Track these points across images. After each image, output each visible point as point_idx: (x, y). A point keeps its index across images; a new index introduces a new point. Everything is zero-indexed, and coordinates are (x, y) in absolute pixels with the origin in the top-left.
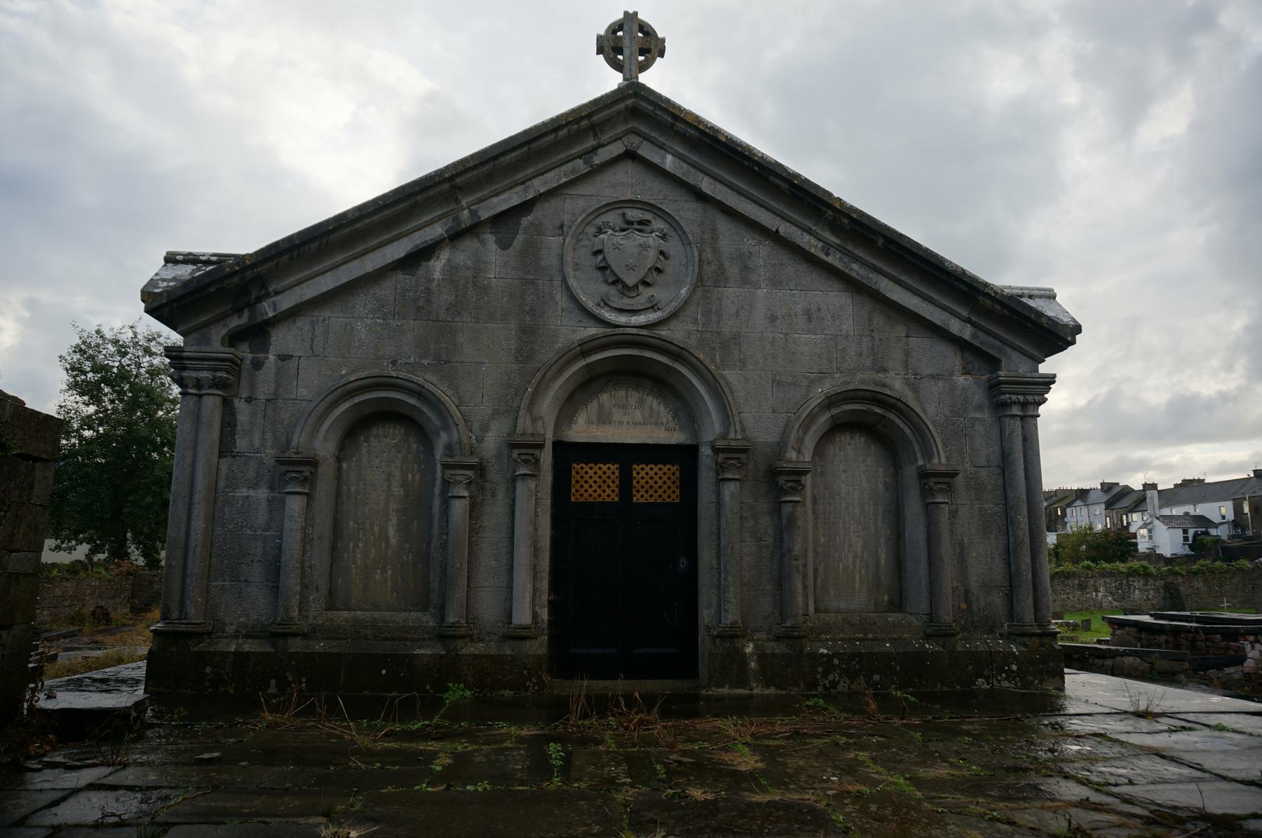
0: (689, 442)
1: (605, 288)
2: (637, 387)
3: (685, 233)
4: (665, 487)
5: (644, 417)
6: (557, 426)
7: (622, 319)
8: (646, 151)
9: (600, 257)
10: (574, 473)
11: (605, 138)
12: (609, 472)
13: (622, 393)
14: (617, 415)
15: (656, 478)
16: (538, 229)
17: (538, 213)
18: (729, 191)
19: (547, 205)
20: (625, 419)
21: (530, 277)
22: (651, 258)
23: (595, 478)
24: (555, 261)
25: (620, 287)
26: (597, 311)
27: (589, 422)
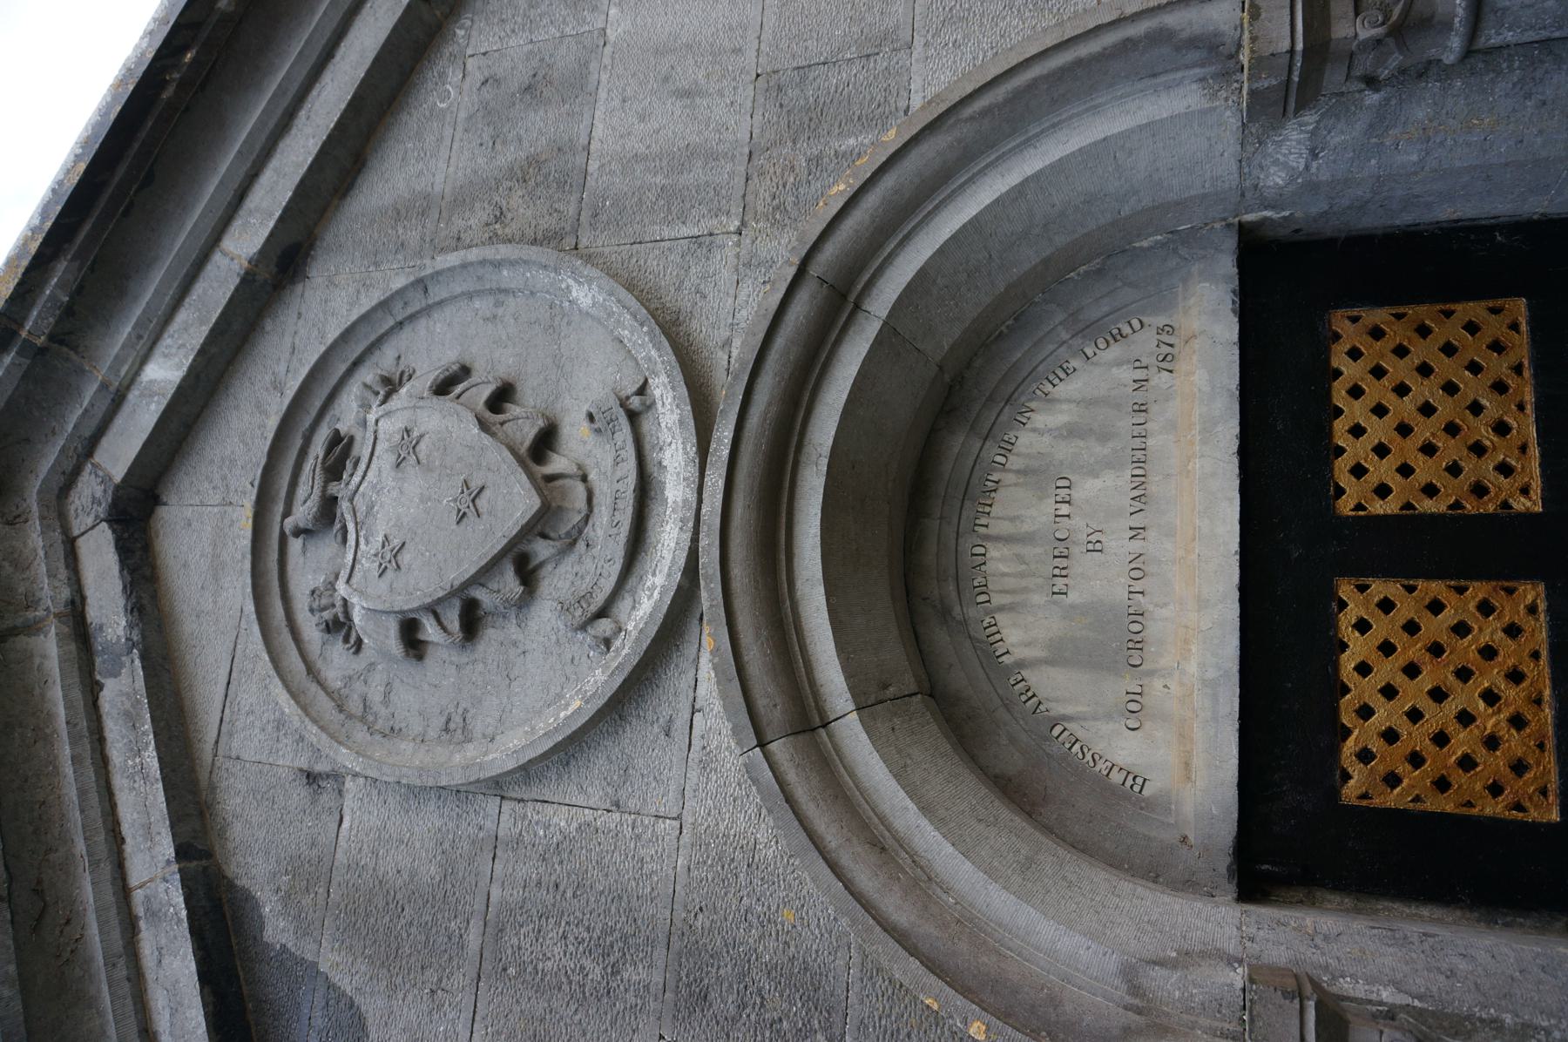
0: (1227, 265)
1: (545, 614)
2: (975, 491)
3: (384, 305)
4: (1445, 368)
5: (1110, 464)
6: (1156, 869)
7: (668, 540)
8: (120, 453)
9: (430, 631)
10: (1393, 799)
11: (50, 592)
12: (1382, 627)
13: (999, 561)
14: (1099, 581)
15: (1405, 408)
16: (311, 873)
17: (256, 862)
18: (274, 163)
19: (237, 831)
20: (1119, 545)
21: (473, 939)
22: (451, 425)
23: (1414, 693)
24: (429, 820)
25: (542, 550)
26: (627, 650)
27: (1135, 710)
